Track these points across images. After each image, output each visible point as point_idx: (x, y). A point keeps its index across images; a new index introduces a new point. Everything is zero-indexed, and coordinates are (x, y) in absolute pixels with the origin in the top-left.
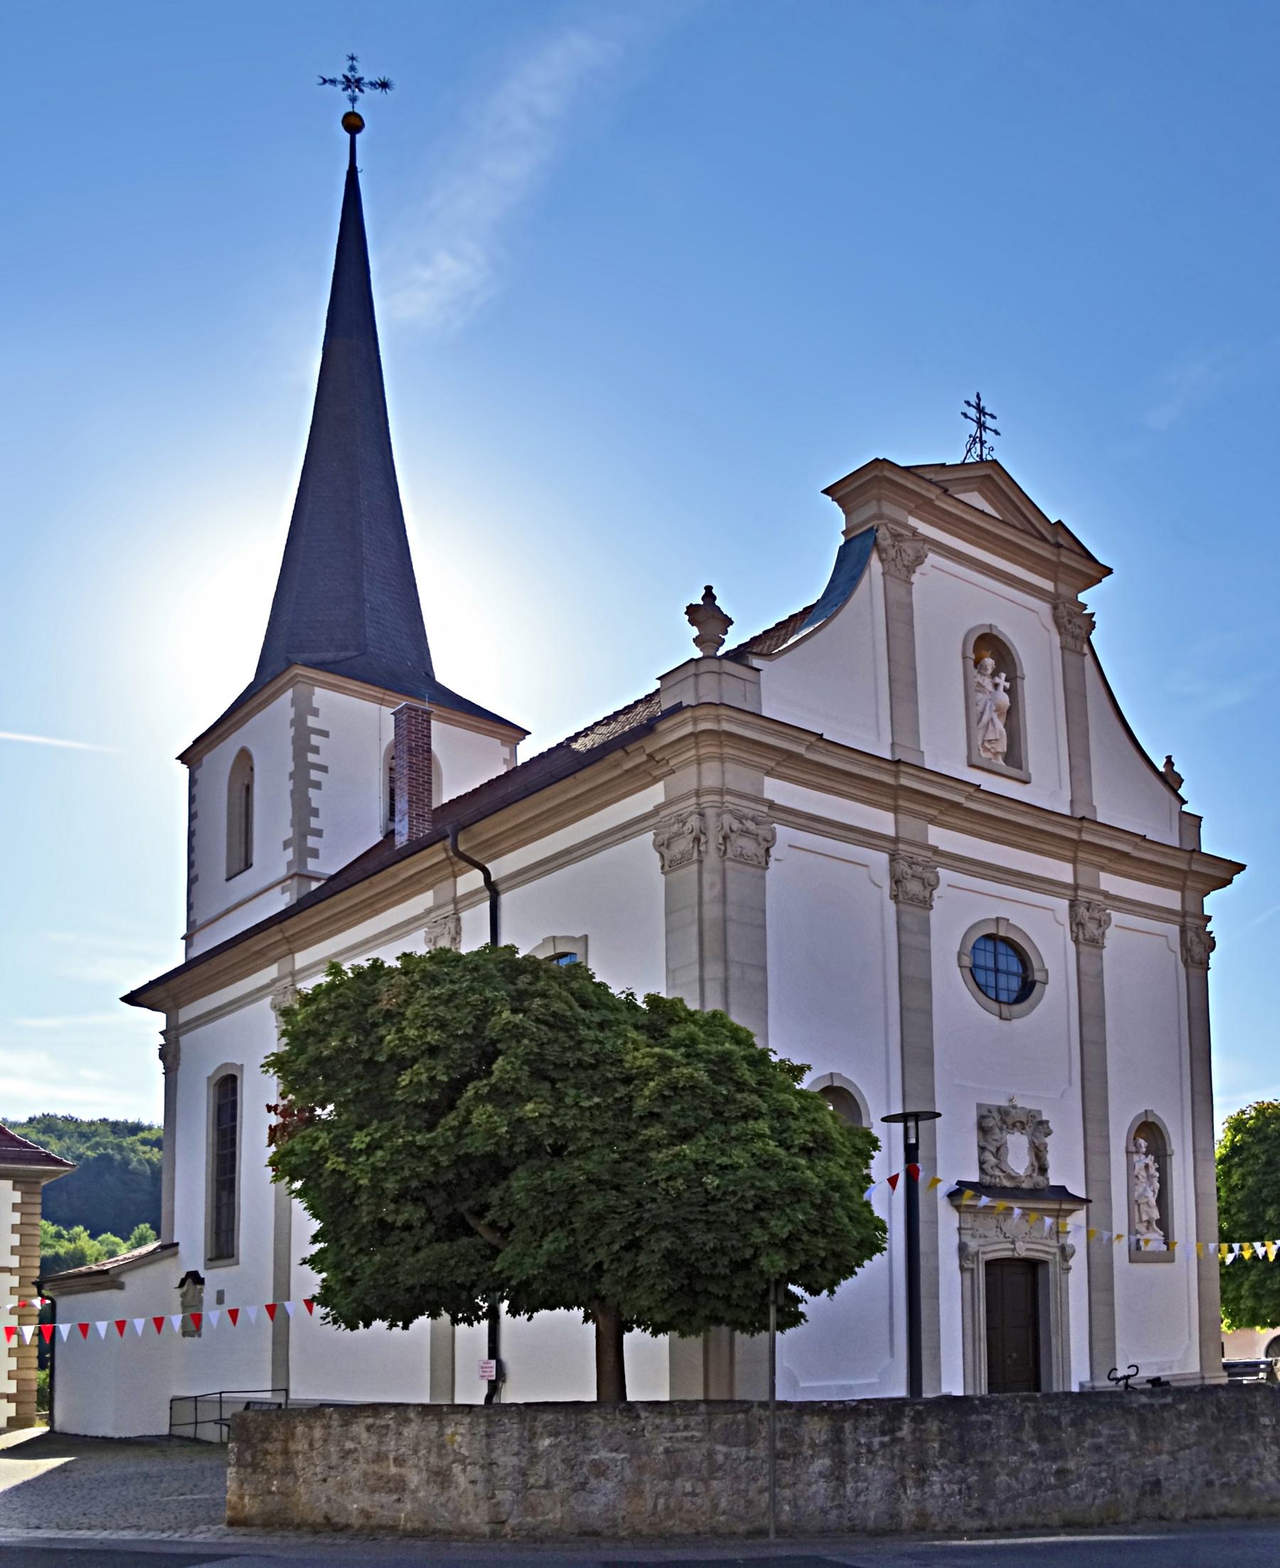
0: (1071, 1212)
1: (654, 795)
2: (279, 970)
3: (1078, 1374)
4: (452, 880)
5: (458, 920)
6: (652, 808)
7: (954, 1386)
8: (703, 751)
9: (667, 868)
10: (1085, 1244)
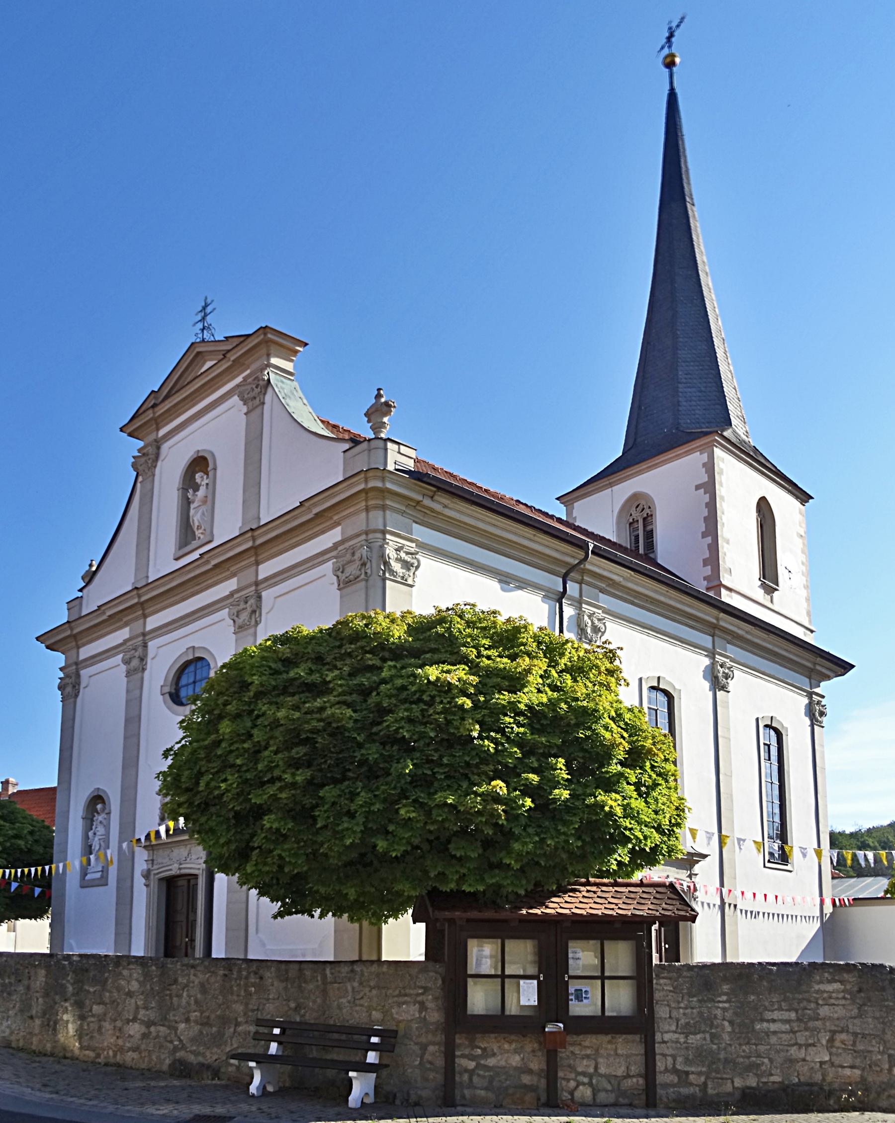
0: (698, 862)
1: (335, 535)
2: (131, 631)
3: (218, 952)
4: (254, 567)
5: (260, 597)
6: (331, 545)
7: (138, 950)
8: (371, 503)
9: (342, 586)
10: (135, 880)
